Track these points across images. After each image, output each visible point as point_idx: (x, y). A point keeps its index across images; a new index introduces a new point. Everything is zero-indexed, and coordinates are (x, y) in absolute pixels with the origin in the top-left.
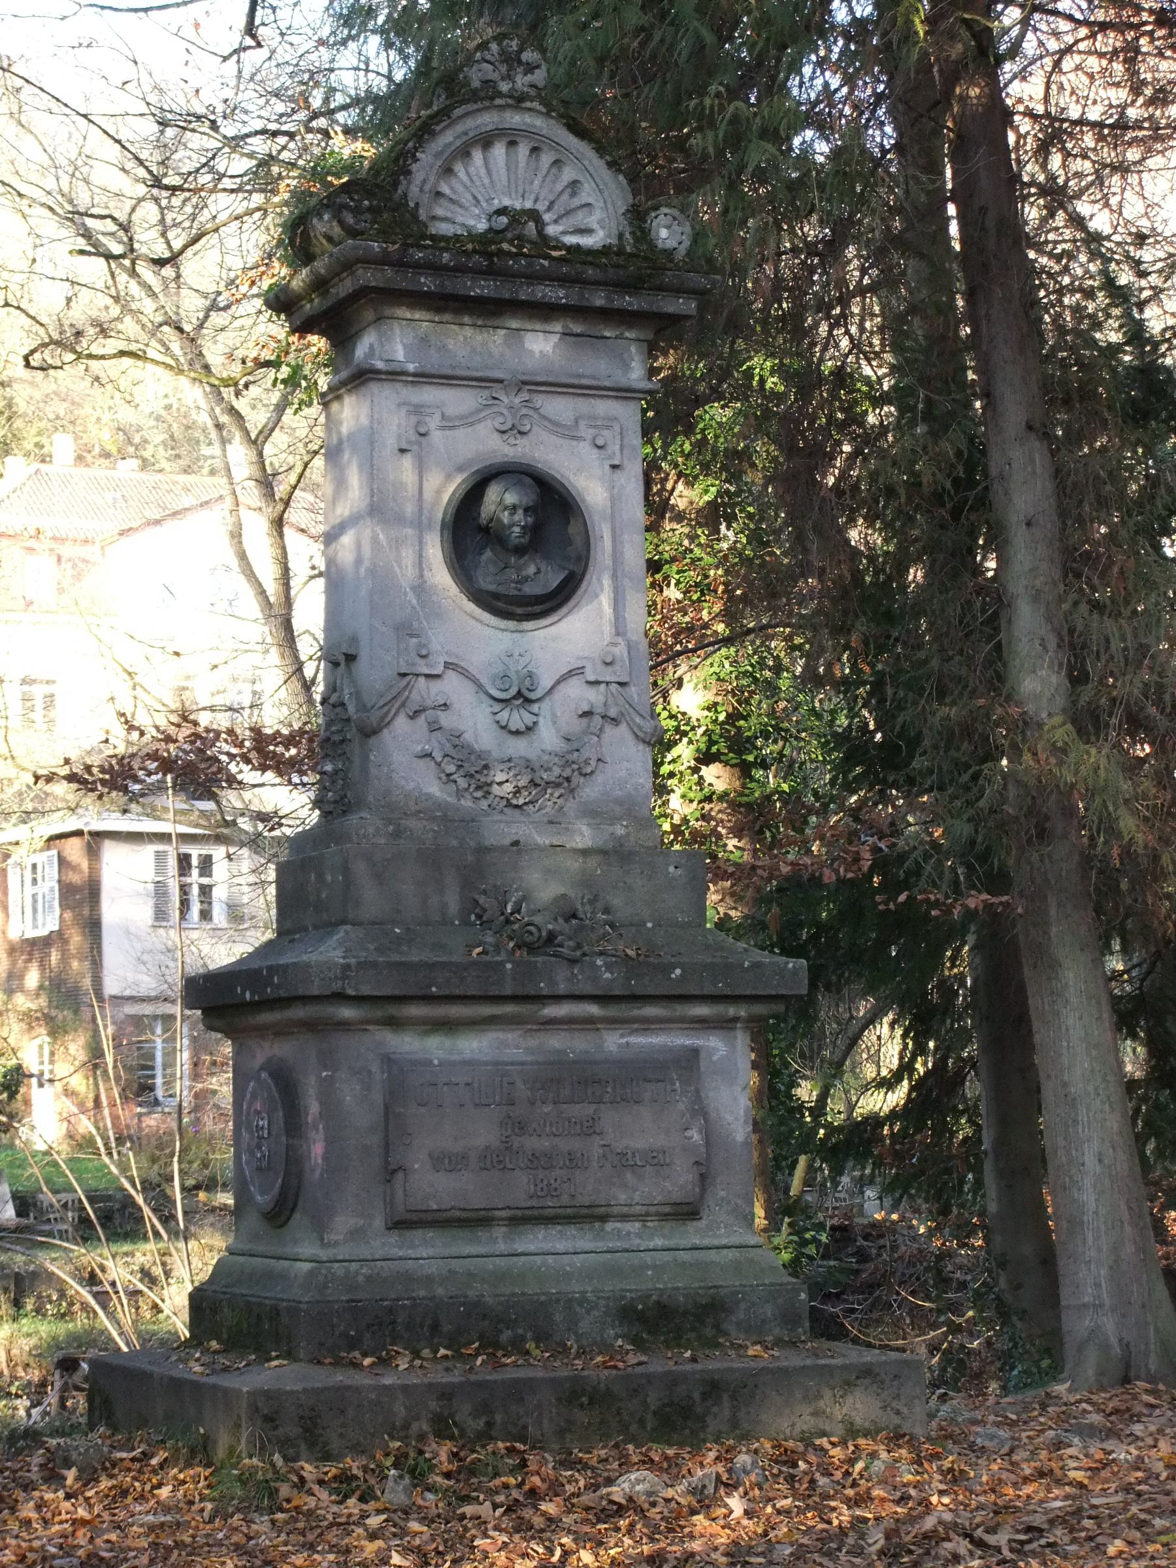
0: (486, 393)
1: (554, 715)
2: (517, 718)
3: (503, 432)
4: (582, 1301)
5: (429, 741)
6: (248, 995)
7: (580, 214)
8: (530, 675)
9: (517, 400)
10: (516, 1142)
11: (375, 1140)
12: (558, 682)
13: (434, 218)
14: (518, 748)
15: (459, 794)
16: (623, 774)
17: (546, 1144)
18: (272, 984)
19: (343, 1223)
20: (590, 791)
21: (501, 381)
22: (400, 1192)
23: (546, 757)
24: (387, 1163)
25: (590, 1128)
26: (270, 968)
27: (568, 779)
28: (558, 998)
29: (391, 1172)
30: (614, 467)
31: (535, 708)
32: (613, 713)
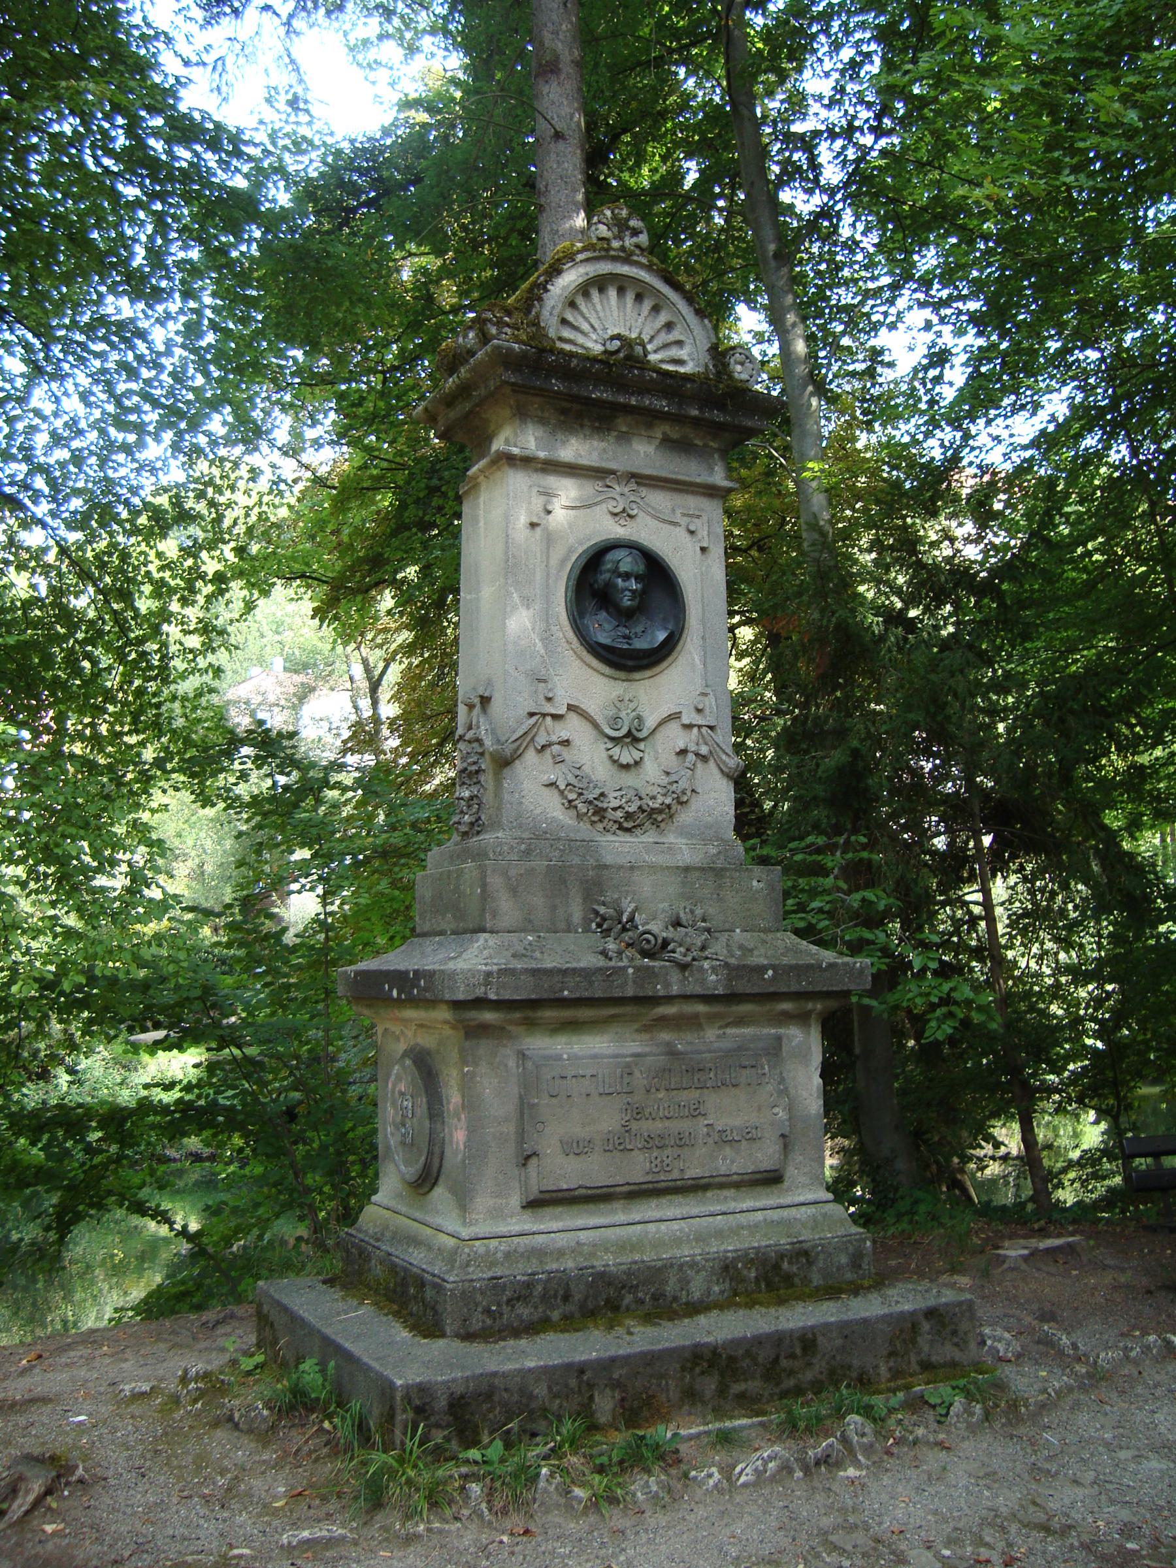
2: (626, 756)
4: (693, 1265)
8: (639, 718)
10: (634, 1126)
11: (510, 1128)
12: (660, 725)
17: (659, 1125)
19: (482, 1202)
20: (685, 817)
21: (613, 472)
25: (697, 1113)
26: (416, 972)
28: (669, 999)
30: (703, 549)
31: (642, 746)
32: (704, 750)
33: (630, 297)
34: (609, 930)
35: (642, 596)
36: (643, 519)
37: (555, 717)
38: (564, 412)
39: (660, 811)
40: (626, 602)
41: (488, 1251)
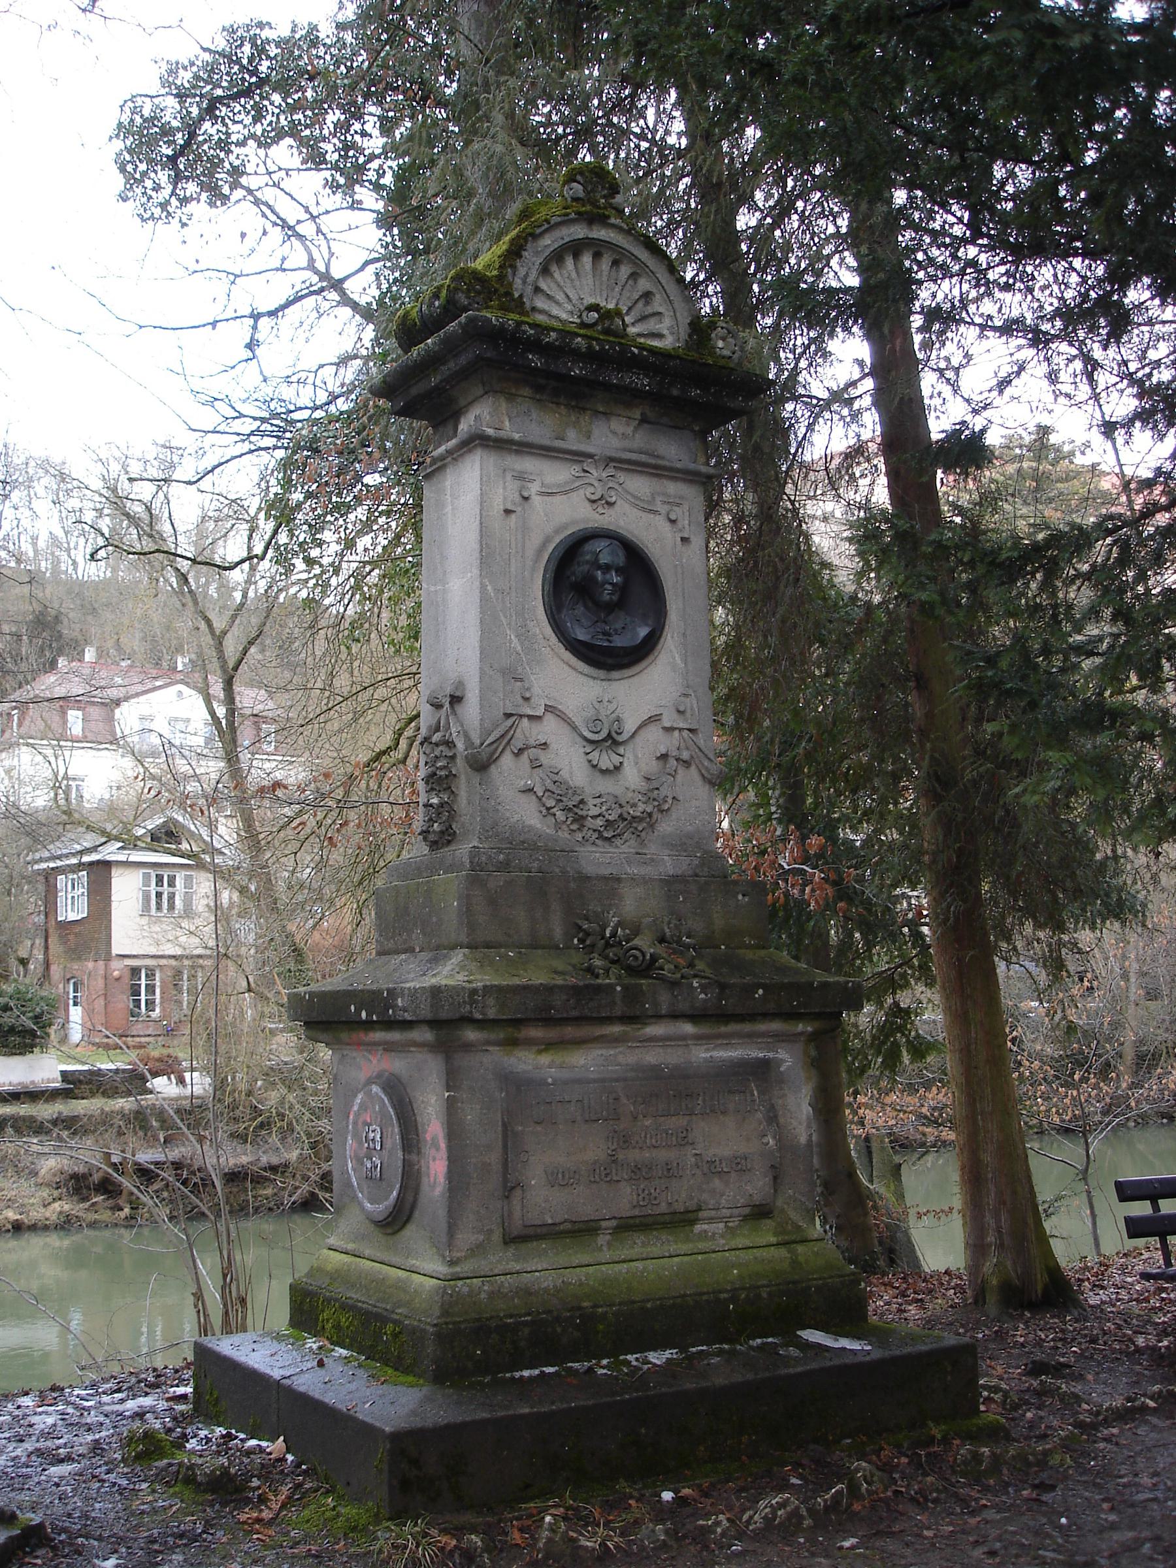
0: (577, 467)
1: (636, 757)
2: (606, 760)
3: (594, 502)
5: (530, 777)
6: (364, 1015)
7: (652, 321)
8: (618, 720)
9: (604, 475)
11: (494, 1158)
12: (640, 728)
13: (534, 309)
14: (606, 786)
15: (558, 826)
16: (693, 810)
18: (394, 1007)
20: (666, 827)
21: (591, 456)
22: (518, 1208)
23: (630, 795)
24: (505, 1181)
25: (684, 1141)
27: (650, 815)
29: (510, 1188)
30: (684, 540)
31: (621, 750)
32: (685, 755)
33: (605, 263)
34: (593, 946)
35: (623, 590)
36: (622, 507)
37: (531, 718)
38: (539, 389)
39: (641, 820)
40: (606, 595)
41: (471, 1291)
